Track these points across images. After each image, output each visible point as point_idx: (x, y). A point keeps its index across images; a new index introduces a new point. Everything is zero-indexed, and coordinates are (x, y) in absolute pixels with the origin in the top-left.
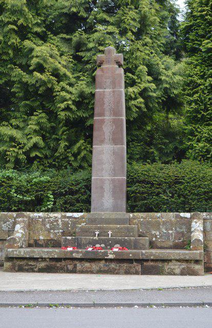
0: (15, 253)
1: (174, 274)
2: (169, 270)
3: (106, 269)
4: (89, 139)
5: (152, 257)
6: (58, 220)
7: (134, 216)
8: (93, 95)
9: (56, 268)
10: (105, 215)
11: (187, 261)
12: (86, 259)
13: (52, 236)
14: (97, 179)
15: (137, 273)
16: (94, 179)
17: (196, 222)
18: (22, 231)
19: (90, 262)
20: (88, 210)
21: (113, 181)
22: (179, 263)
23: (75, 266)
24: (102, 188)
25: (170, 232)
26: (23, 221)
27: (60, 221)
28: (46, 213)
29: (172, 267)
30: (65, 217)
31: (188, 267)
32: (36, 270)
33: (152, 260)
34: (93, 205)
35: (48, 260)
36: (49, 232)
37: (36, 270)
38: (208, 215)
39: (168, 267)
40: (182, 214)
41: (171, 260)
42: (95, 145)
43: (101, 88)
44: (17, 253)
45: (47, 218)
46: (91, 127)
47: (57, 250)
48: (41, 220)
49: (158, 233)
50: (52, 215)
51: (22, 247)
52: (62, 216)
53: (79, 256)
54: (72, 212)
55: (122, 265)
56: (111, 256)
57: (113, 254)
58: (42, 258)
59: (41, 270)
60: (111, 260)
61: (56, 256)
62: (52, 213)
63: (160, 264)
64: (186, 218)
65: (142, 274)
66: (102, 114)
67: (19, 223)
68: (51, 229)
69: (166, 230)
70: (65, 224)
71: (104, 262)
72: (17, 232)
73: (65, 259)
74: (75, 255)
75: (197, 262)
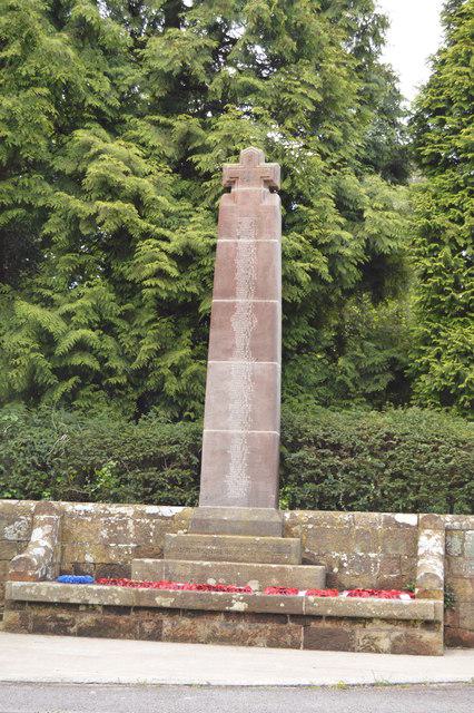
0: (28, 591)
1: (378, 651)
2: (366, 641)
3: (227, 632)
5: (329, 612)
6: (126, 522)
7: (293, 516)
9: (117, 628)
11: (406, 622)
12: (184, 610)
13: (113, 556)
14: (215, 433)
15: (295, 645)
16: (207, 434)
17: (429, 536)
18: (46, 543)
19: (190, 617)
21: (250, 438)
22: (389, 627)
24: (225, 453)
25: (372, 555)
26: (50, 521)
27: (131, 522)
29: (374, 634)
30: (142, 514)
31: (407, 636)
32: (72, 630)
33: (330, 618)
35: (100, 609)
36: (107, 546)
37: (72, 630)
38: (457, 520)
39: (364, 634)
40: (401, 518)
42: (213, 359)
43: (230, 236)
45: (104, 515)
48: (89, 519)
50: (114, 509)
51: (44, 579)
52: (136, 512)
55: (262, 626)
56: (239, 606)
57: (242, 601)
58: (87, 605)
60: (238, 614)
61: (117, 602)
63: (346, 627)
64: (408, 526)
65: (308, 647)
66: (231, 293)
67: (42, 524)
68: (111, 541)
70: (143, 531)
72: (37, 544)
73: (138, 609)
74: (160, 601)
75: (428, 624)
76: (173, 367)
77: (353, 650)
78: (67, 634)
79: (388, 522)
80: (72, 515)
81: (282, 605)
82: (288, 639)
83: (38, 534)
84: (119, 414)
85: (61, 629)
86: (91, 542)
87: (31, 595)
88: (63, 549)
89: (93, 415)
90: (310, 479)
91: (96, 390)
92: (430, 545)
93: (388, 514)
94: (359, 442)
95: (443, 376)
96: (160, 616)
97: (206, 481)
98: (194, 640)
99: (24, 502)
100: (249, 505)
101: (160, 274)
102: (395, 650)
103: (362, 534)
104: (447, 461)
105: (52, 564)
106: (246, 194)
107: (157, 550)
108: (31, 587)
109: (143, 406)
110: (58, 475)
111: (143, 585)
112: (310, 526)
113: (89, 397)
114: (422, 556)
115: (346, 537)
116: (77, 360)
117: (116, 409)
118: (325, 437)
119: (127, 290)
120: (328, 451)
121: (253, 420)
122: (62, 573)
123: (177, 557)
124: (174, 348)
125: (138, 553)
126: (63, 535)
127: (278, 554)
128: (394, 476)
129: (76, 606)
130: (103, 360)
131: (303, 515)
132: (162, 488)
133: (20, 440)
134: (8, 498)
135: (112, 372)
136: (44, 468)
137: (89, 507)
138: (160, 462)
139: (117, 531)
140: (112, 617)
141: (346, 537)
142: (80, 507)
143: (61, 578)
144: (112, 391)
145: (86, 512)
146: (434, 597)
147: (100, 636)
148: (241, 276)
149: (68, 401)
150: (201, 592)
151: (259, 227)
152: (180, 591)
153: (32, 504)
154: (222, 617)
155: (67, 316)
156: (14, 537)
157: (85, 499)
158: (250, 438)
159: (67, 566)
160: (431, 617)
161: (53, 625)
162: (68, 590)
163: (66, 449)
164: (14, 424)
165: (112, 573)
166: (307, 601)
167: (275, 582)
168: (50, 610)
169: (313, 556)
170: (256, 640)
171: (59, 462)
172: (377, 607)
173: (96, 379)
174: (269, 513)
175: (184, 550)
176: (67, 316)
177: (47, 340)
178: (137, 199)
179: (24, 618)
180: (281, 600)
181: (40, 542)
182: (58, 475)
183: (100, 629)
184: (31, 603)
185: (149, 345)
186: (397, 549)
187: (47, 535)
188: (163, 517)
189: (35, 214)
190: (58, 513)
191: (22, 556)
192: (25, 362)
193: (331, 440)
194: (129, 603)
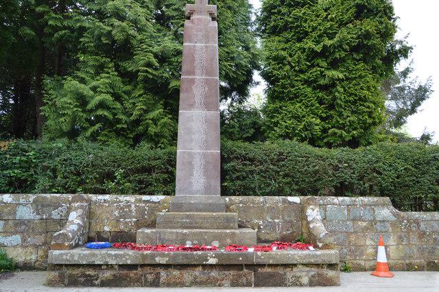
0: (64, 257)
1: (301, 285)
3: (204, 278)
4: (173, 111)
5: (271, 262)
6: (130, 206)
7: (230, 200)
8: (179, 53)
9: (128, 279)
10: (199, 198)
11: (317, 265)
12: (174, 265)
13: (122, 227)
14: (184, 152)
15: (248, 285)
16: (180, 153)
18: (79, 221)
19: (179, 269)
20: (170, 192)
21: (205, 155)
22: (308, 269)
23: (158, 276)
24: (190, 163)
25: (277, 221)
26: (81, 207)
27: (133, 206)
28: (115, 196)
29: (298, 274)
30: (140, 201)
31: (319, 274)
32: (96, 282)
33: (270, 266)
34: (179, 185)
35: (116, 267)
36: (118, 221)
37: (96, 282)
39: (292, 274)
40: (290, 199)
41: (295, 265)
42: (184, 109)
43: (190, 42)
44: (68, 258)
45: (116, 202)
46: (177, 91)
47: (130, 253)
48: (107, 205)
49: (261, 223)
50: (123, 198)
51: (77, 246)
52: (136, 200)
53: (163, 261)
54: (149, 194)
55: (227, 273)
56: (212, 261)
57: (214, 258)
58: (107, 265)
59: (104, 284)
60: (212, 266)
61: (129, 262)
62: (123, 196)
63: (280, 271)
64: (296, 203)
65: (257, 285)
66: (192, 73)
67: (76, 209)
68: (121, 217)
69: (272, 219)
70: (141, 211)
71: (200, 268)
72: (72, 222)
73: (142, 266)
74: (158, 260)
76: (152, 119)
77: (286, 285)
78: (93, 285)
79: (284, 201)
80: (96, 202)
81: (241, 259)
82: (244, 280)
83: (73, 216)
84: (123, 145)
85: (89, 282)
86: (108, 219)
87: (67, 260)
88: (90, 223)
89: (108, 145)
90: (238, 178)
91: (110, 131)
92: (313, 213)
93: (284, 197)
94: (265, 158)
95: (286, 127)
96: (158, 270)
97: (180, 180)
98: (181, 284)
99: (65, 195)
100: (205, 194)
101: (149, 65)
102: (312, 284)
103: (271, 209)
104: (314, 166)
105: (83, 235)
106: (199, 20)
107: (149, 222)
108: (67, 255)
109: (137, 140)
110: (87, 178)
111: (146, 249)
112: (241, 205)
113: (106, 135)
114: (312, 221)
115: (261, 211)
116: (100, 112)
117: (121, 142)
118: (247, 154)
119: (129, 77)
120: (248, 162)
121: (206, 145)
122: (90, 240)
123: (164, 227)
124: (153, 110)
125: (139, 225)
126: (89, 215)
127: (227, 223)
128: (286, 176)
129: (100, 266)
130: (115, 115)
131: (236, 199)
132: (151, 184)
133: (63, 157)
134: (55, 193)
135: (119, 121)
136: (78, 174)
137: (107, 197)
138: (148, 170)
139: (125, 212)
140: (125, 272)
141: (261, 211)
142: (101, 197)
143: (89, 244)
144: (119, 133)
145: (105, 200)
146: (332, 248)
147: (117, 286)
148: (197, 63)
149: (94, 137)
150: (185, 252)
151: (207, 38)
152: (172, 253)
153: (70, 196)
154: (200, 268)
155: (94, 89)
156: (58, 217)
157: (103, 192)
158: (205, 155)
159: (93, 234)
160: (334, 262)
161: (83, 279)
162: (94, 255)
163: (92, 162)
164: (60, 148)
165: (123, 239)
166: (257, 255)
167: (229, 241)
168: (81, 269)
169: (243, 223)
170: (223, 282)
171: (88, 170)
172: (301, 258)
173: (110, 124)
174: (216, 197)
175: (169, 223)
176: (94, 89)
177: (82, 100)
178: (135, 22)
179: (62, 277)
180: (241, 255)
181: (75, 220)
182: (87, 178)
183: (116, 281)
184: (66, 265)
185: (140, 106)
186: (290, 217)
187: (79, 216)
188: (153, 202)
189: (76, 34)
190: (87, 201)
191: (61, 232)
192: (69, 112)
193: (251, 155)
194: (137, 262)
